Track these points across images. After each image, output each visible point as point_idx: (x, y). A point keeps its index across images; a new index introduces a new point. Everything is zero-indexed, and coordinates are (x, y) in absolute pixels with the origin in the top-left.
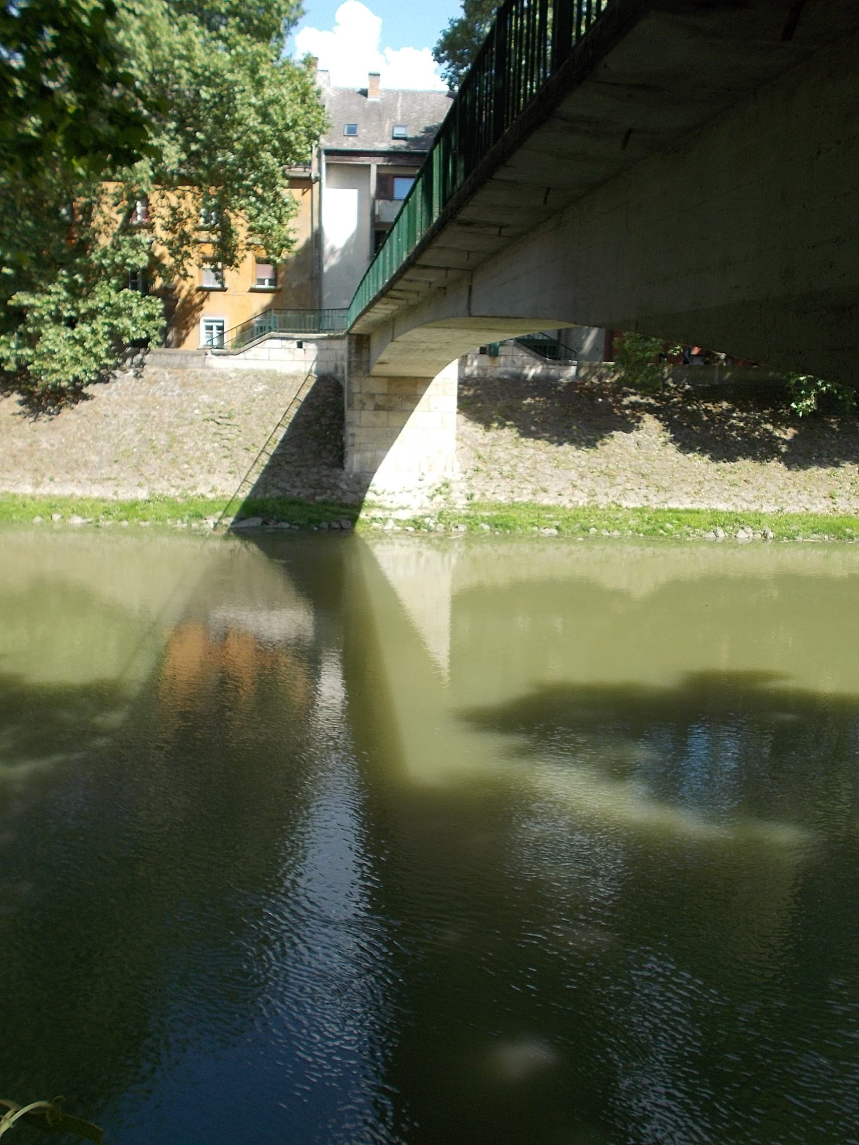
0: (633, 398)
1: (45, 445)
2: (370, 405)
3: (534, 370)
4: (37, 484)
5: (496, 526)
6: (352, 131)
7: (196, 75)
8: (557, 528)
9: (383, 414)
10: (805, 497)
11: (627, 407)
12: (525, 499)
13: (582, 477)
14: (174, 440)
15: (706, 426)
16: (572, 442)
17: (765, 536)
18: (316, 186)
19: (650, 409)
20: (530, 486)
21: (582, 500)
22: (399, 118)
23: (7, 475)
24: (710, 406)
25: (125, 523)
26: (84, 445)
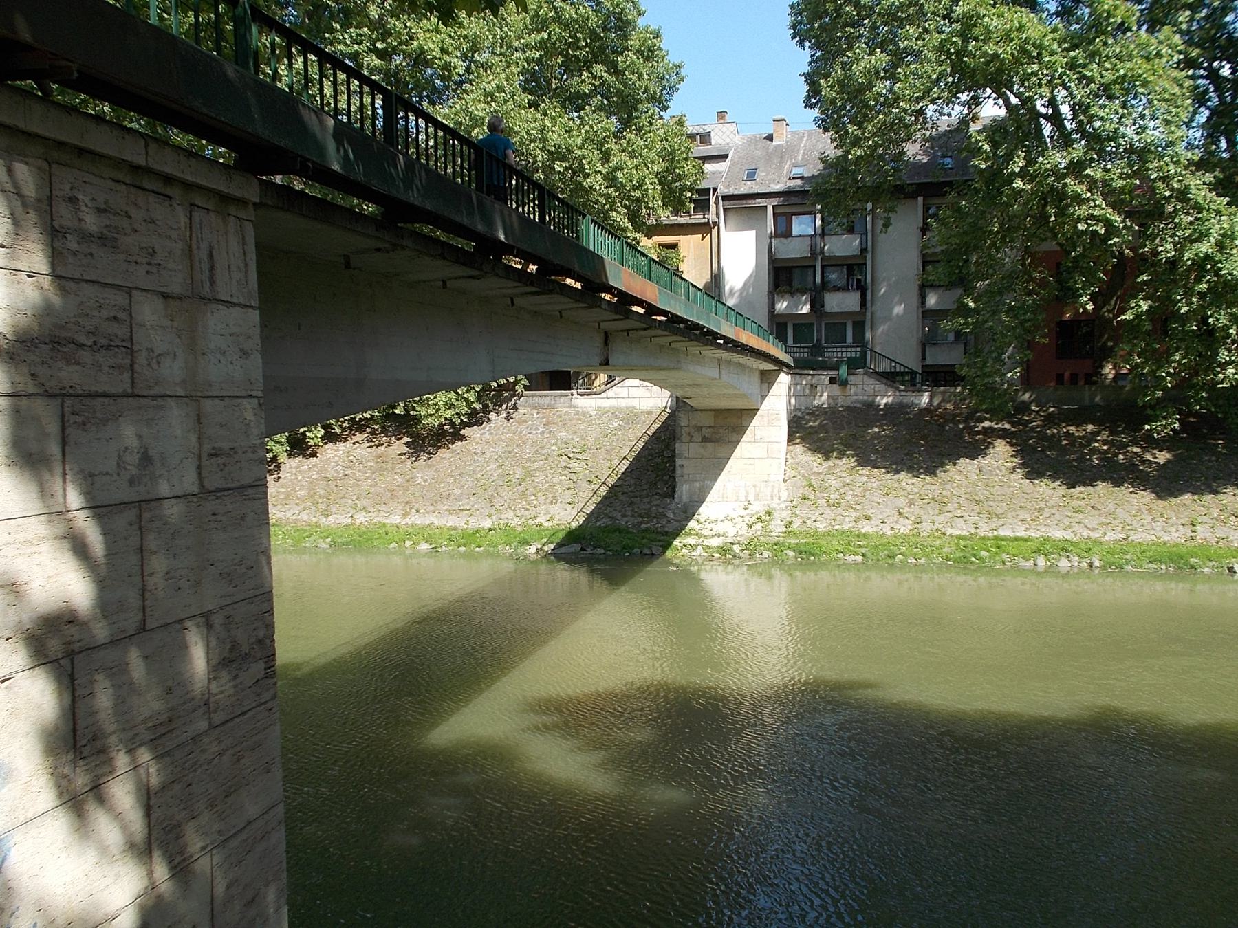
0: (987, 424)
1: (420, 481)
2: (697, 437)
3: (885, 399)
4: (404, 516)
5: (801, 552)
6: (751, 175)
7: (551, 153)
8: (864, 555)
9: (710, 445)
10: (1158, 526)
11: (978, 433)
12: (845, 527)
13: (911, 504)
14: (528, 473)
15: (1064, 451)
16: (911, 469)
17: (1091, 565)
18: (714, 231)
19: (1004, 434)
20: (853, 514)
21: (905, 527)
22: (800, 158)
23: (383, 507)
24: (1072, 429)
25: (463, 549)
26: (451, 480)
